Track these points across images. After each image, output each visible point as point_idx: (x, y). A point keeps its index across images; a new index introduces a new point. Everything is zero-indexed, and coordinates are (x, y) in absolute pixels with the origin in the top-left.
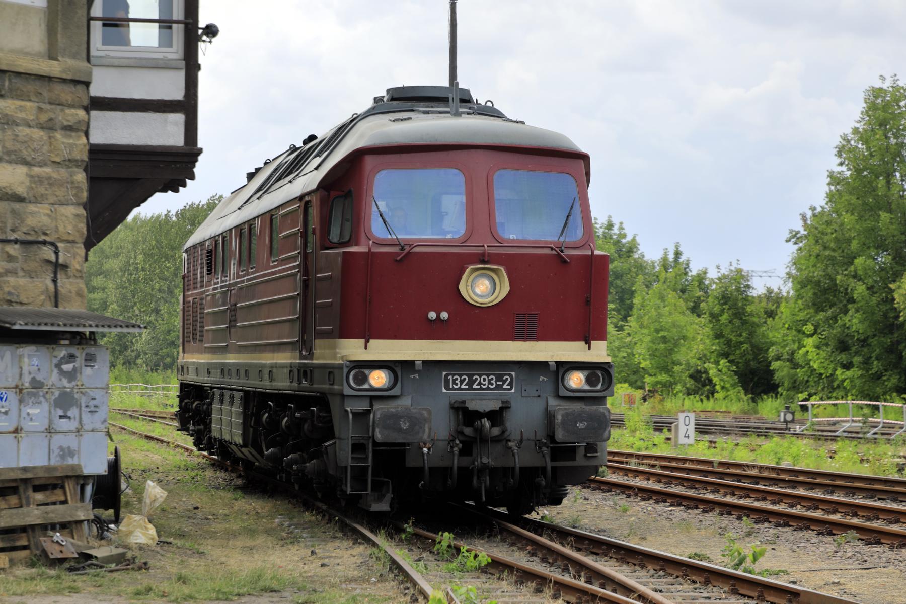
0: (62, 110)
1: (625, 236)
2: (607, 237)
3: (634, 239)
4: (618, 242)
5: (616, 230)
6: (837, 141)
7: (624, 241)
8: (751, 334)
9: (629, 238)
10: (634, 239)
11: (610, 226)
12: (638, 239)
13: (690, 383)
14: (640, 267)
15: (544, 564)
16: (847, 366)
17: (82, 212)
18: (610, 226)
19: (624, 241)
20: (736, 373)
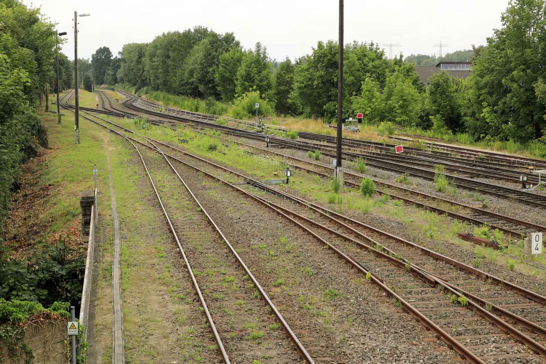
0: (485, 206)
1: (379, 49)
2: (371, 49)
3: (383, 51)
4: (376, 52)
5: (375, 46)
6: (331, 40)
7: (112, 58)
8: (450, 101)
9: (381, 50)
10: (383, 51)
11: (372, 45)
12: (384, 51)
13: (418, 120)
14: (386, 62)
15: (267, 55)
16: (506, 122)
17: (285, 60)
18: (372, 45)
19: (378, 51)
20: (444, 120)
